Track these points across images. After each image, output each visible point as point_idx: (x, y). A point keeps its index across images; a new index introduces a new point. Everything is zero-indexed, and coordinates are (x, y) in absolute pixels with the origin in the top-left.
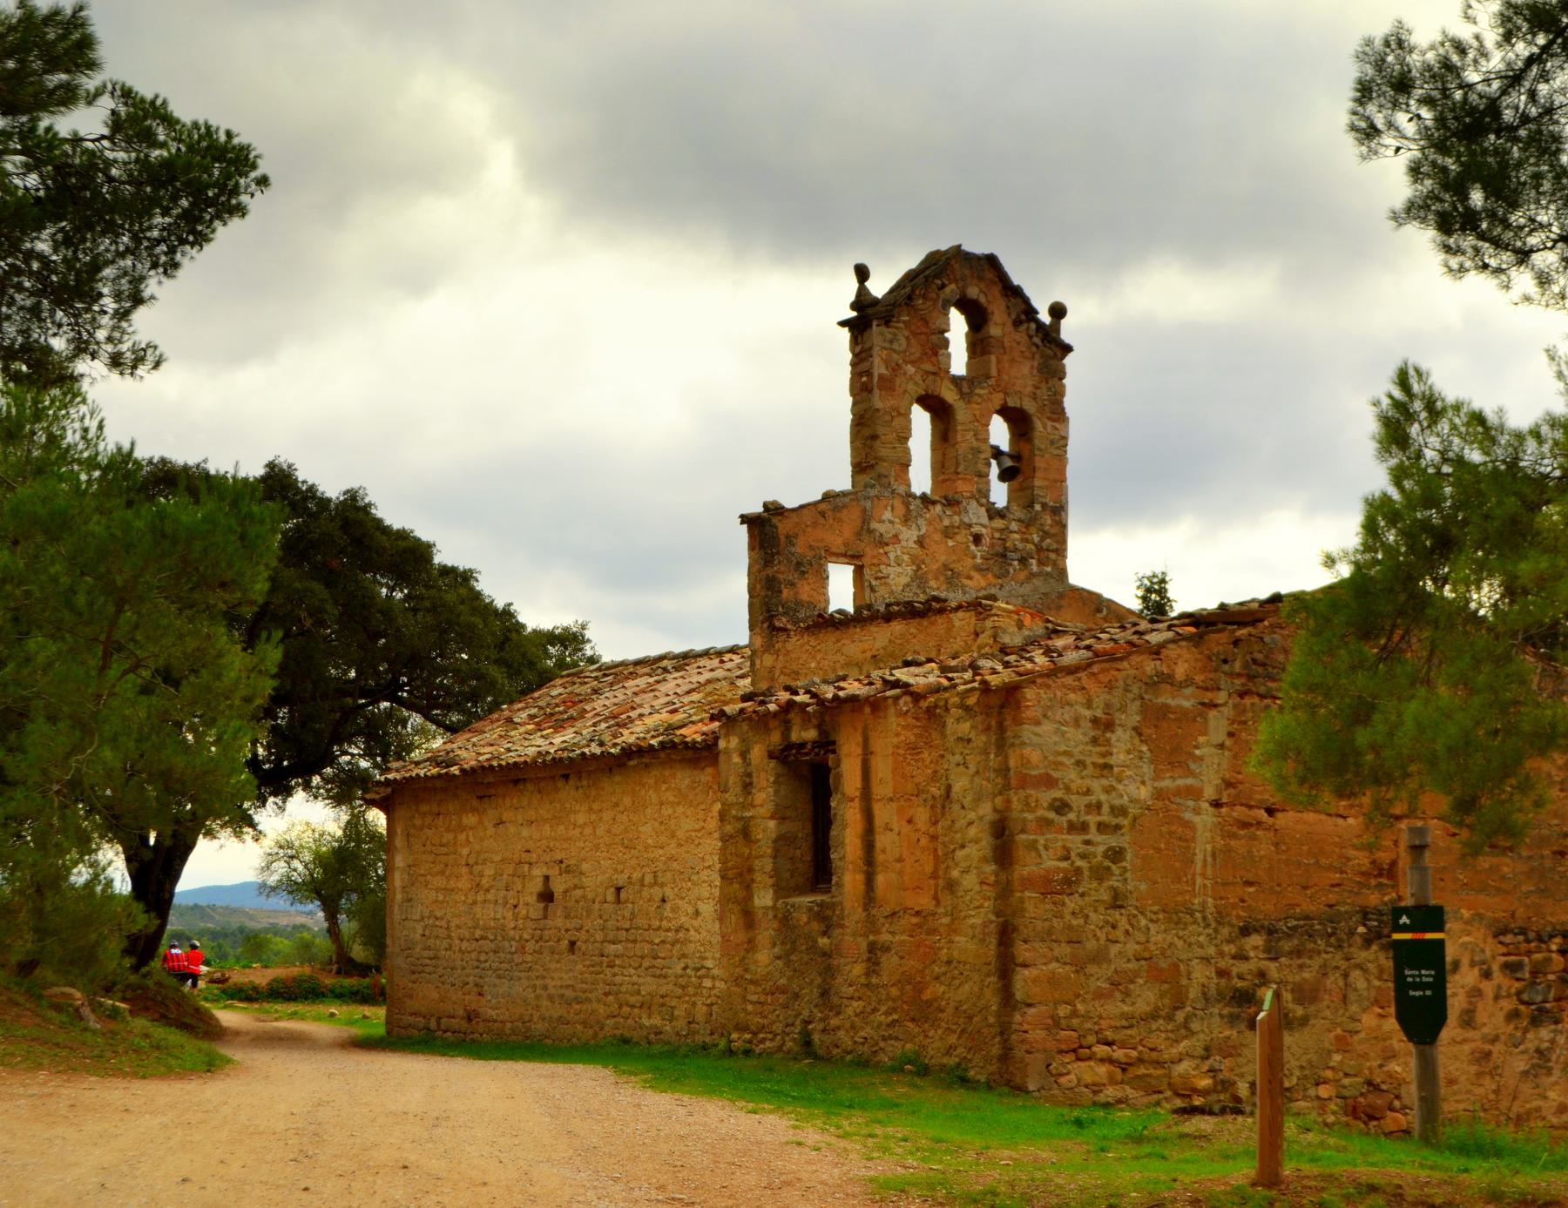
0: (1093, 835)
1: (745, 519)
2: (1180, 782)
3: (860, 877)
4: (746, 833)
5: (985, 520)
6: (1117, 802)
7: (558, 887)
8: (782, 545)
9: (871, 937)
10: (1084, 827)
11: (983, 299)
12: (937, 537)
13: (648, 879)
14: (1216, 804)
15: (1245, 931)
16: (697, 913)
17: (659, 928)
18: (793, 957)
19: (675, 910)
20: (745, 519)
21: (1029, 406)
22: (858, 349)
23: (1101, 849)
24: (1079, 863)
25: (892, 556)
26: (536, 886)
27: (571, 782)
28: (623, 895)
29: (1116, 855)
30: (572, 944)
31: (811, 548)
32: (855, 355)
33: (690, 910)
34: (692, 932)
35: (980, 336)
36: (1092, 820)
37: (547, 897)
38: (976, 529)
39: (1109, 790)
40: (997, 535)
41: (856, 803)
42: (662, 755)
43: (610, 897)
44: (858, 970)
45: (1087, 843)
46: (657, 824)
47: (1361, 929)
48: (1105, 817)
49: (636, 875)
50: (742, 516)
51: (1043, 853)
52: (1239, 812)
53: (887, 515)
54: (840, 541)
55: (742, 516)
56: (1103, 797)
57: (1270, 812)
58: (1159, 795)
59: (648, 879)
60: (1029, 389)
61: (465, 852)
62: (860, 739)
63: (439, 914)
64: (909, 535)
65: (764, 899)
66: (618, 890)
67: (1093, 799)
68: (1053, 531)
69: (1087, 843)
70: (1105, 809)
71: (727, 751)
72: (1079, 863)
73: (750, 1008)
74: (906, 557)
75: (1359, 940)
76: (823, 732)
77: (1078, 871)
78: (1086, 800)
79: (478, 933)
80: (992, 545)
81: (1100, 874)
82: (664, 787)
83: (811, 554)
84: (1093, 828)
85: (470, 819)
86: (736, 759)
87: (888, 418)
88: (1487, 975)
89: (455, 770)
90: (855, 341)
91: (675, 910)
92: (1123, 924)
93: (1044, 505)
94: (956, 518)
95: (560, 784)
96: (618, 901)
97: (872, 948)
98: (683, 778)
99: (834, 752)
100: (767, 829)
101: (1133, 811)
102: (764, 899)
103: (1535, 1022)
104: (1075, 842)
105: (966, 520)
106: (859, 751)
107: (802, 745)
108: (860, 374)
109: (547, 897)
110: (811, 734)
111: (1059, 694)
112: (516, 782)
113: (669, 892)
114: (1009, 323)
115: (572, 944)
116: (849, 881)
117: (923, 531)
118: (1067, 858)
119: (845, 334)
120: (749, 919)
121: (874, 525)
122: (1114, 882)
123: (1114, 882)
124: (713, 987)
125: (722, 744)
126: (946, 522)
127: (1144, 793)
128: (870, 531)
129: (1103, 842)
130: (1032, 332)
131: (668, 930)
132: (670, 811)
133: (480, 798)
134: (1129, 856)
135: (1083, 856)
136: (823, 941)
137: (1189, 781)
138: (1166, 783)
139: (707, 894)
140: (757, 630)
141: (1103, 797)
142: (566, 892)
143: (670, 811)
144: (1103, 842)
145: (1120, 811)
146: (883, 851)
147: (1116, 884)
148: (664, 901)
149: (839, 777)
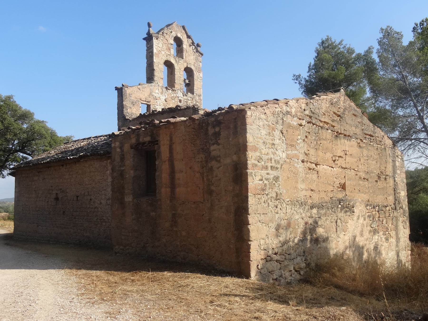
0: (269, 171)
1: (117, 88)
2: (293, 152)
3: (168, 190)
4: (122, 175)
5: (182, 96)
6: (276, 158)
7: (60, 196)
8: (128, 97)
9: (173, 212)
10: (266, 168)
11: (181, 37)
12: (170, 99)
13: (86, 194)
14: (303, 161)
15: (312, 207)
16: (101, 203)
17: (89, 207)
18: (140, 220)
19: (94, 202)
20: (117, 88)
21: (193, 68)
22: (148, 46)
23: (272, 176)
24: (265, 182)
25: (158, 103)
26: (54, 196)
27: (64, 167)
28: (79, 198)
29: (276, 179)
30: (64, 212)
31: (136, 98)
32: (147, 47)
33: (99, 202)
34: (99, 209)
35: (180, 48)
36: (269, 165)
37: (57, 199)
38: (180, 98)
39: (274, 154)
40: (185, 100)
41: (167, 163)
42: (91, 157)
43: (75, 199)
44: (167, 225)
45: (268, 174)
46: (89, 178)
47: (340, 206)
48: (273, 164)
49: (83, 193)
50: (116, 87)
51: (254, 177)
52: (309, 164)
53: (157, 91)
54: (144, 97)
55: (116, 87)
56: (272, 156)
57: (316, 165)
58: (288, 157)
59: (86, 194)
60: (193, 63)
61: (34, 187)
62: (169, 139)
63: (27, 204)
64: (163, 98)
65: (129, 199)
66: (77, 197)
67: (269, 157)
68: (198, 101)
69: (268, 174)
70: (273, 161)
71: (115, 148)
72: (265, 182)
73: (123, 237)
74: (162, 104)
75: (339, 209)
76: (152, 136)
77: (265, 185)
78: (267, 157)
79: (37, 209)
80: (184, 103)
81: (272, 186)
82: (91, 167)
83: (136, 100)
84: (269, 168)
85: (36, 178)
86: (118, 150)
87: (157, 65)
88: (365, 219)
89: (31, 164)
90: (148, 43)
91: (94, 202)
92: (279, 206)
93: (196, 94)
94: (175, 94)
95: (61, 167)
96: (77, 200)
97: (174, 215)
98: (97, 164)
99: (157, 144)
100: (130, 174)
101: (281, 162)
102: (129, 199)
103: (374, 234)
104: (264, 172)
105: (177, 95)
106: (168, 143)
107: (144, 143)
108: (149, 53)
109: (57, 199)
110: (148, 139)
111: (258, 114)
112: (49, 167)
113: (92, 197)
114: (188, 45)
115: (64, 212)
116: (164, 191)
117: (166, 97)
118: (262, 180)
119: (145, 42)
120: (122, 203)
121: (153, 94)
122: (276, 189)
123: (276, 189)
124: (106, 225)
125: (113, 145)
126: (172, 95)
127: (284, 155)
128: (153, 95)
129: (273, 173)
130: (194, 48)
131: (92, 208)
132: (93, 174)
133: (38, 172)
134: (280, 179)
135: (267, 179)
136: (153, 214)
137: (296, 152)
138: (289, 152)
139: (104, 198)
140: (120, 120)
141: (272, 156)
142: (62, 198)
143: (93, 174)
144: (273, 173)
145: (277, 162)
146: (179, 179)
147: (277, 190)
148: (91, 200)
149: (159, 153)
